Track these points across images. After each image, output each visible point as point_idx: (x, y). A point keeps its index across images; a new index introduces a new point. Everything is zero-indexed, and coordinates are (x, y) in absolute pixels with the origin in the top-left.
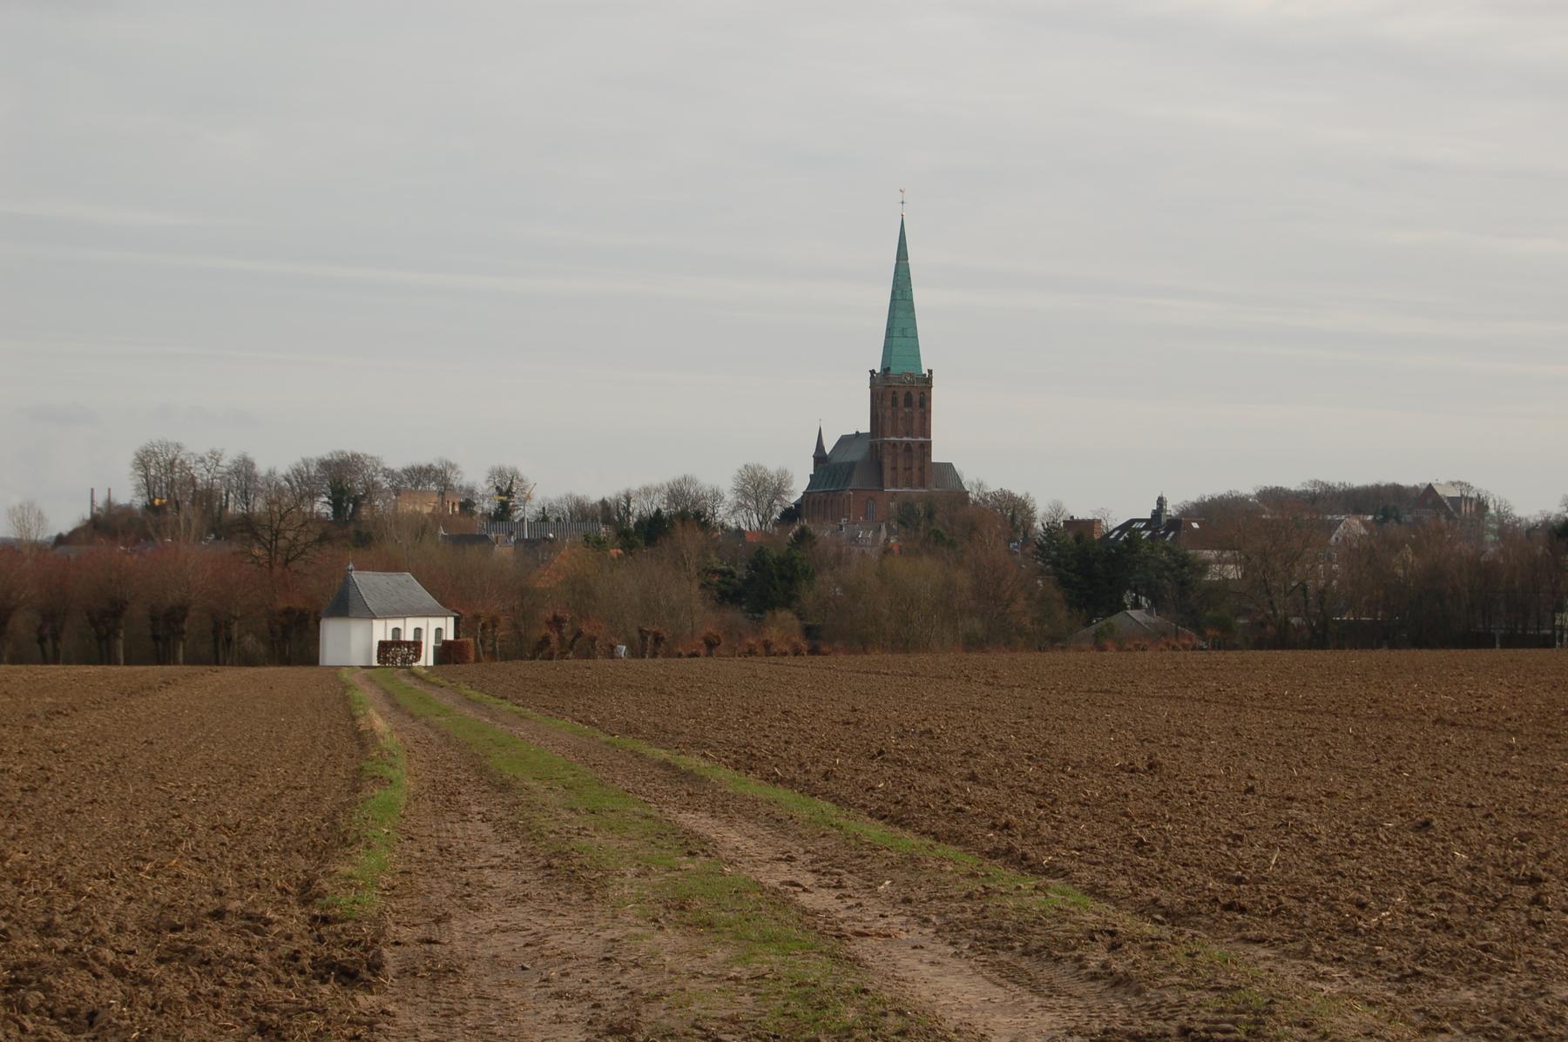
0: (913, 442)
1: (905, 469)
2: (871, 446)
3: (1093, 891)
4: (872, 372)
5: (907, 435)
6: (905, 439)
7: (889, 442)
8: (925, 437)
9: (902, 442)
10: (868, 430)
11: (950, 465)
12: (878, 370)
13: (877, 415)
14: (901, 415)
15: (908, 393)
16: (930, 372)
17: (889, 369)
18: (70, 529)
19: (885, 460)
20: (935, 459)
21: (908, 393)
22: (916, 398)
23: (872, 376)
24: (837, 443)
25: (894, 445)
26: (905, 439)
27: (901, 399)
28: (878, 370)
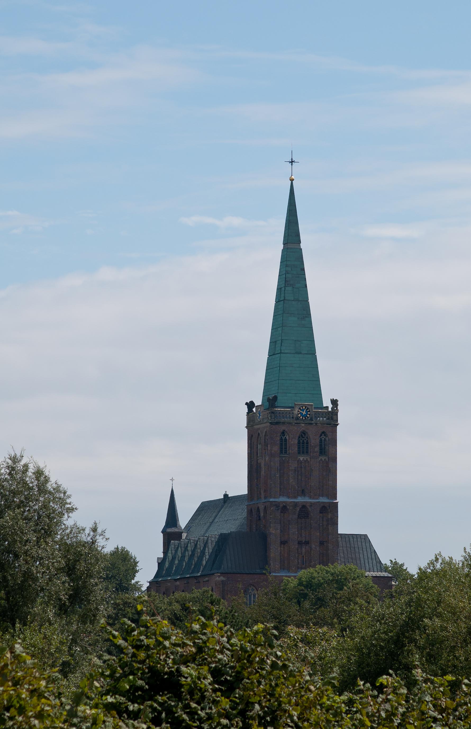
0: (312, 505)
1: (300, 543)
2: (250, 512)
3: (280, 488)
4: (250, 405)
5: (303, 493)
6: (300, 499)
7: (277, 505)
8: (328, 497)
9: (296, 504)
10: (244, 491)
11: (365, 537)
12: (258, 402)
13: (259, 466)
14: (293, 465)
15: (304, 433)
16: (335, 402)
17: (275, 398)
18: (247, 409)
19: (272, 531)
20: (341, 530)
21: (304, 433)
22: (314, 440)
23: (250, 410)
24: (272, 353)
25: (284, 508)
26: (300, 499)
27: (293, 442)
28: (258, 402)
